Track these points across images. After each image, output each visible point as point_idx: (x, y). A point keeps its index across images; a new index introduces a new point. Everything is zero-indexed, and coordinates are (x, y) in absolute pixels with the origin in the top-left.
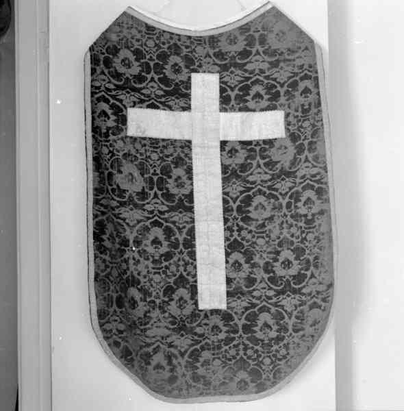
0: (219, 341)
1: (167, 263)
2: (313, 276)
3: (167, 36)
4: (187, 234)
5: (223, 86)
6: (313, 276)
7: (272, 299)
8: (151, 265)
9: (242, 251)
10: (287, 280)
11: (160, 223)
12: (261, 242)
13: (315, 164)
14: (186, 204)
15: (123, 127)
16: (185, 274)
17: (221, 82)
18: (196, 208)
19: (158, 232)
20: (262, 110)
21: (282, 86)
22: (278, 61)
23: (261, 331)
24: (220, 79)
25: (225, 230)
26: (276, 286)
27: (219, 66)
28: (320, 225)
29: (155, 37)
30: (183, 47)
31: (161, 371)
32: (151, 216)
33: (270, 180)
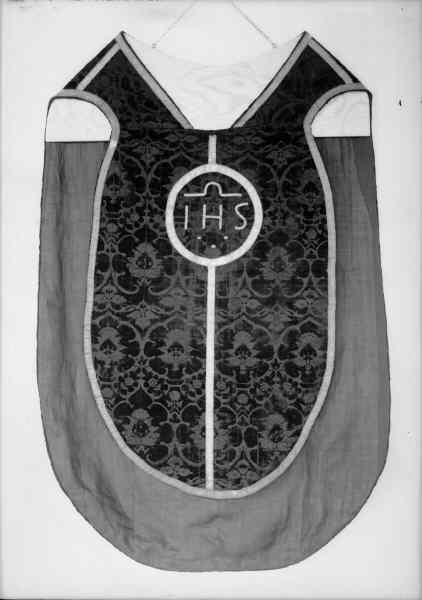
9: (149, 407)
29: (248, 390)
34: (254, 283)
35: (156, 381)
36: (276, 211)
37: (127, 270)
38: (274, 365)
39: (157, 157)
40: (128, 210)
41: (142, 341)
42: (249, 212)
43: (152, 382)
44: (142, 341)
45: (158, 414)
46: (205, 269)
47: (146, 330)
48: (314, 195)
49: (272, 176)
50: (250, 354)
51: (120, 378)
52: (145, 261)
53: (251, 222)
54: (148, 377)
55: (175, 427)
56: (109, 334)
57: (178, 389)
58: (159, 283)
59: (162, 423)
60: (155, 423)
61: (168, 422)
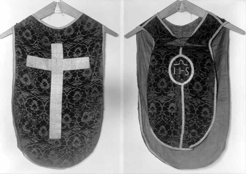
0: (58, 147)
1: (38, 115)
2: (96, 122)
3: (44, 28)
4: (47, 104)
5: (65, 49)
6: (96, 122)
7: (79, 131)
8: (32, 115)
10: (86, 123)
11: (36, 99)
12: (77, 109)
13: (98, 77)
14: (47, 93)
15: (25, 60)
16: (45, 120)
17: (63, 48)
18: (51, 95)
19: (35, 102)
20: (79, 57)
21: (88, 46)
22: (87, 36)
23: (74, 143)
24: (63, 46)
25: (62, 105)
26: (81, 126)
27: (63, 41)
28: (99, 101)
30: (49, 33)
31: (35, 154)
32: (33, 95)
33: (82, 85)
34: (190, 91)
36: (198, 71)
37: (157, 86)
39: (165, 53)
40: (157, 69)
41: (162, 106)
42: (190, 70)
43: (70, 106)
44: (162, 106)
45: (167, 127)
46: (181, 86)
47: (163, 103)
48: (210, 67)
49: (197, 61)
50: (188, 111)
51: (38, 116)
52: (162, 84)
53: (190, 73)
54: (164, 116)
55: (172, 131)
56: (152, 105)
57: (173, 120)
58: (167, 90)
59: (169, 130)
60: (166, 130)
61: (170, 129)
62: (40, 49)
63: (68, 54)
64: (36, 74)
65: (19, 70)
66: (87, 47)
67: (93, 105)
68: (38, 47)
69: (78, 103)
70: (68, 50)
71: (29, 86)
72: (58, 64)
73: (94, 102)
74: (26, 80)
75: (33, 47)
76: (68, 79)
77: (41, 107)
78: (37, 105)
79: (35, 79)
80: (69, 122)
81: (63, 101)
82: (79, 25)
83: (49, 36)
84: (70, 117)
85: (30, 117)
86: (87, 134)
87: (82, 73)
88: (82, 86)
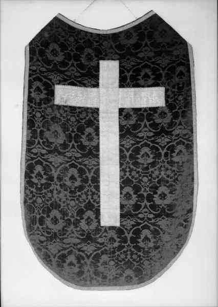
4: (94, 173)
19: (74, 172)
20: (149, 86)
21: (163, 69)
23: (143, 241)
25: (120, 171)
32: (69, 160)
33: (153, 136)
35: (135, 172)
38: (128, 246)
62: (79, 74)
63: (127, 80)
64: (75, 120)
65: (43, 120)
66: (161, 71)
67: (176, 176)
68: (76, 72)
69: (147, 168)
70: (128, 71)
71: (61, 145)
72: (109, 97)
73: (178, 170)
74: (55, 222)
75: (66, 73)
76: (130, 125)
77: (84, 179)
78: (77, 175)
79: (73, 129)
80: (132, 201)
81: (121, 164)
82: (146, 29)
83: (93, 47)
84: (134, 194)
85: (65, 200)
86: (163, 227)
87: (154, 116)
88: (153, 139)
